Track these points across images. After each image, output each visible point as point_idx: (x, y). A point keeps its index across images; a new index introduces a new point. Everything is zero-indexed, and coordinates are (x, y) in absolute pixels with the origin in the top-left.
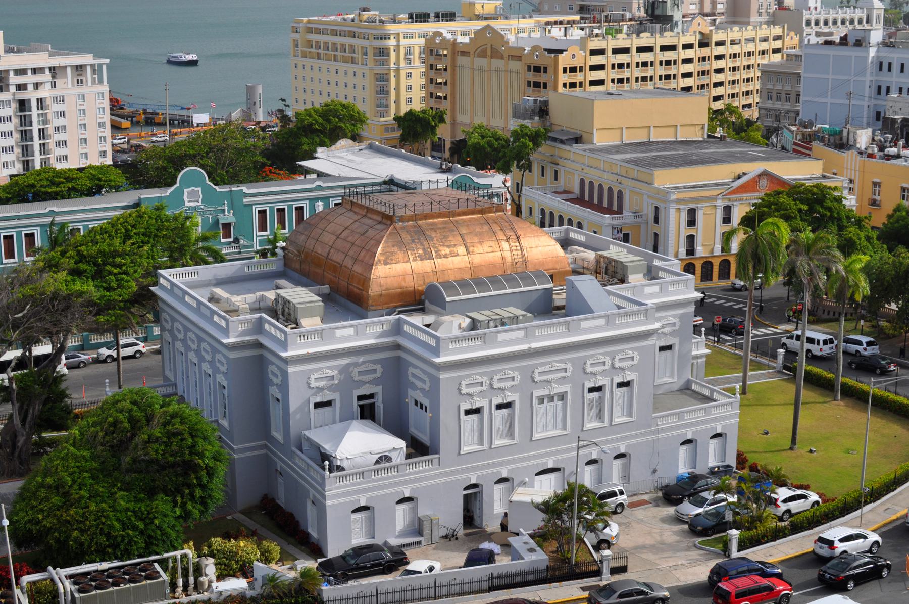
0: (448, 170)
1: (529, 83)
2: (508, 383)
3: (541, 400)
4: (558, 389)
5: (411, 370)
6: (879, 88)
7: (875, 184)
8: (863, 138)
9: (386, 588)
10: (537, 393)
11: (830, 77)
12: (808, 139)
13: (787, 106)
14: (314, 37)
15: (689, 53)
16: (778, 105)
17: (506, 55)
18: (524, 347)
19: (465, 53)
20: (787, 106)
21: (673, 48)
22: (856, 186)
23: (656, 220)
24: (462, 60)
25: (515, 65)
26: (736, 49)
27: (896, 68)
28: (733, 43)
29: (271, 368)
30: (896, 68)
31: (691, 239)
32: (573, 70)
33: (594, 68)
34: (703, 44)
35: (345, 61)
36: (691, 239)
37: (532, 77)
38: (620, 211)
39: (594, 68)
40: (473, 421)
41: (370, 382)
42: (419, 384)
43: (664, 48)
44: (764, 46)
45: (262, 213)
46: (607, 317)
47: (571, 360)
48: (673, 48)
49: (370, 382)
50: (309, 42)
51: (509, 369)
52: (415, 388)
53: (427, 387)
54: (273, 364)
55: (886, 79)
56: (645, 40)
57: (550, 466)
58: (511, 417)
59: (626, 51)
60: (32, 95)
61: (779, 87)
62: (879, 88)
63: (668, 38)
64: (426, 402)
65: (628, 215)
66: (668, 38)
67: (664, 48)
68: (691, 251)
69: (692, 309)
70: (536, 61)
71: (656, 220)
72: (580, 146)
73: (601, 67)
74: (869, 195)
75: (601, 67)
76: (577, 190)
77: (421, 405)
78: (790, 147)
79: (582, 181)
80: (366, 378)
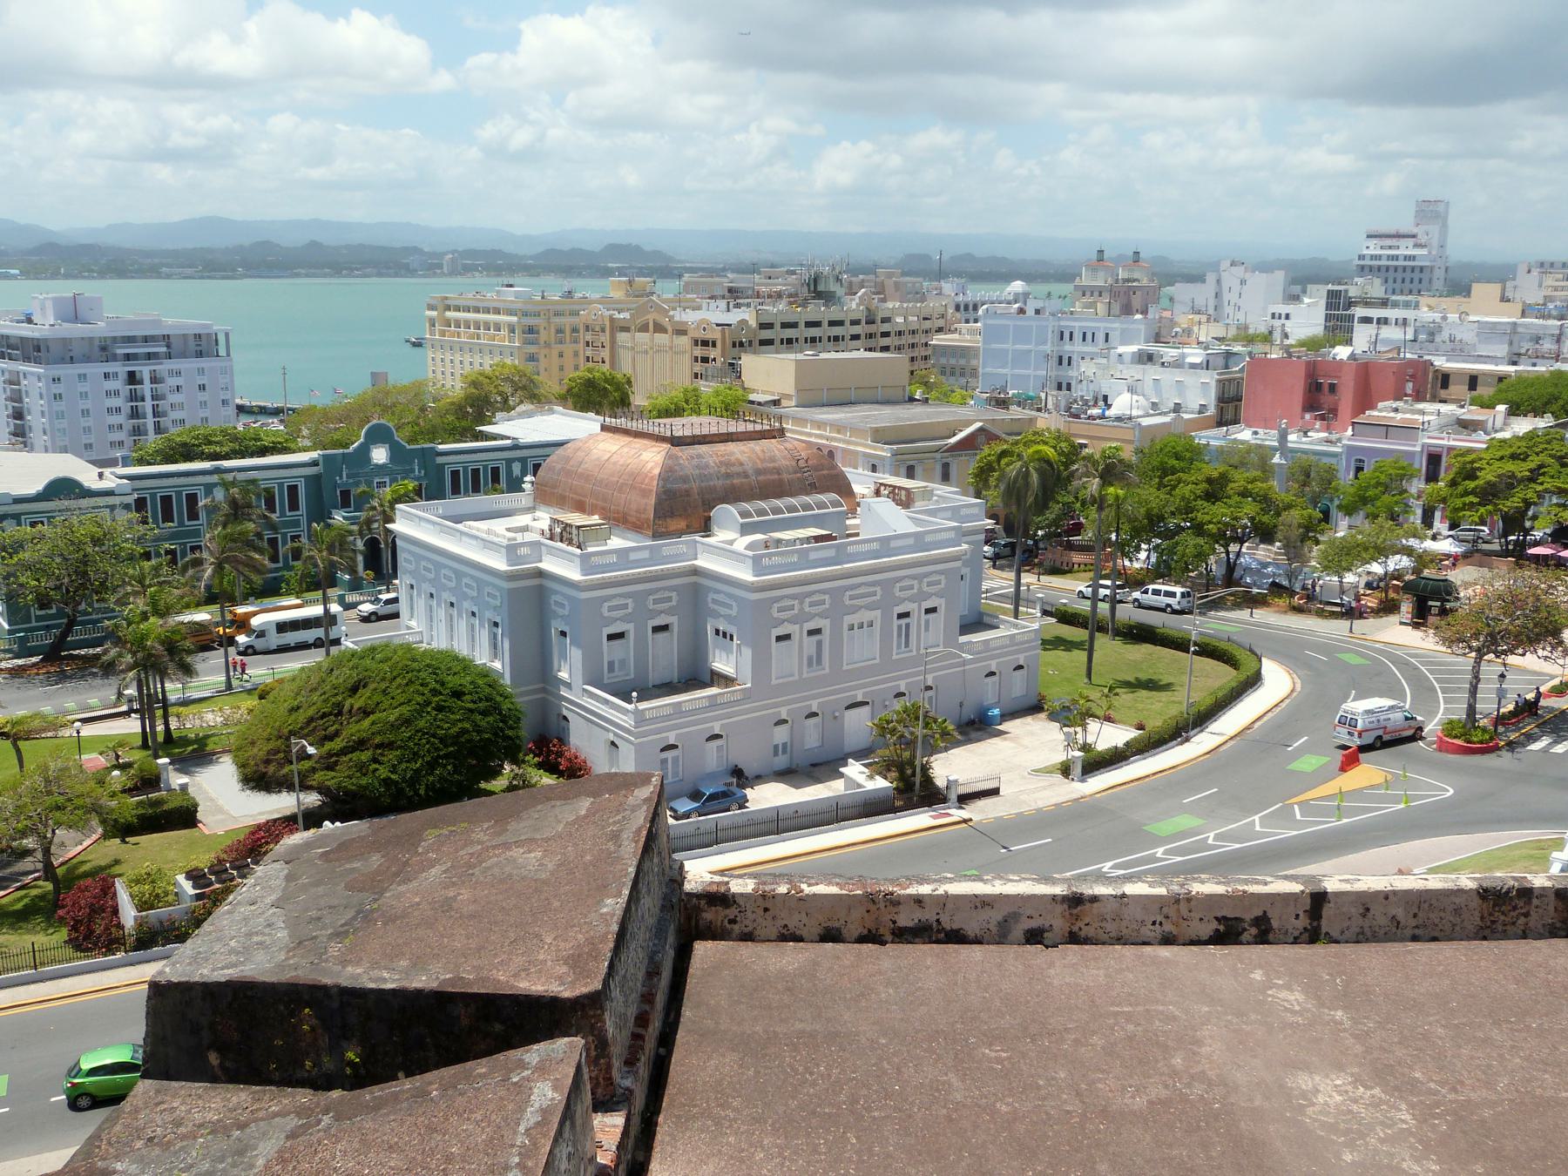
1: (696, 359)
4: (866, 616)
6: (1061, 358)
9: (726, 823)
15: (856, 330)
17: (670, 329)
19: (626, 329)
24: (622, 337)
25: (684, 341)
27: (1078, 336)
30: (1078, 336)
34: (870, 322)
37: (699, 352)
42: (723, 610)
45: (455, 474)
52: (717, 615)
53: (734, 613)
54: (557, 592)
58: (819, 644)
60: (145, 371)
62: (1061, 358)
64: (731, 629)
66: (834, 313)
69: (983, 537)
70: (701, 335)
77: (725, 635)
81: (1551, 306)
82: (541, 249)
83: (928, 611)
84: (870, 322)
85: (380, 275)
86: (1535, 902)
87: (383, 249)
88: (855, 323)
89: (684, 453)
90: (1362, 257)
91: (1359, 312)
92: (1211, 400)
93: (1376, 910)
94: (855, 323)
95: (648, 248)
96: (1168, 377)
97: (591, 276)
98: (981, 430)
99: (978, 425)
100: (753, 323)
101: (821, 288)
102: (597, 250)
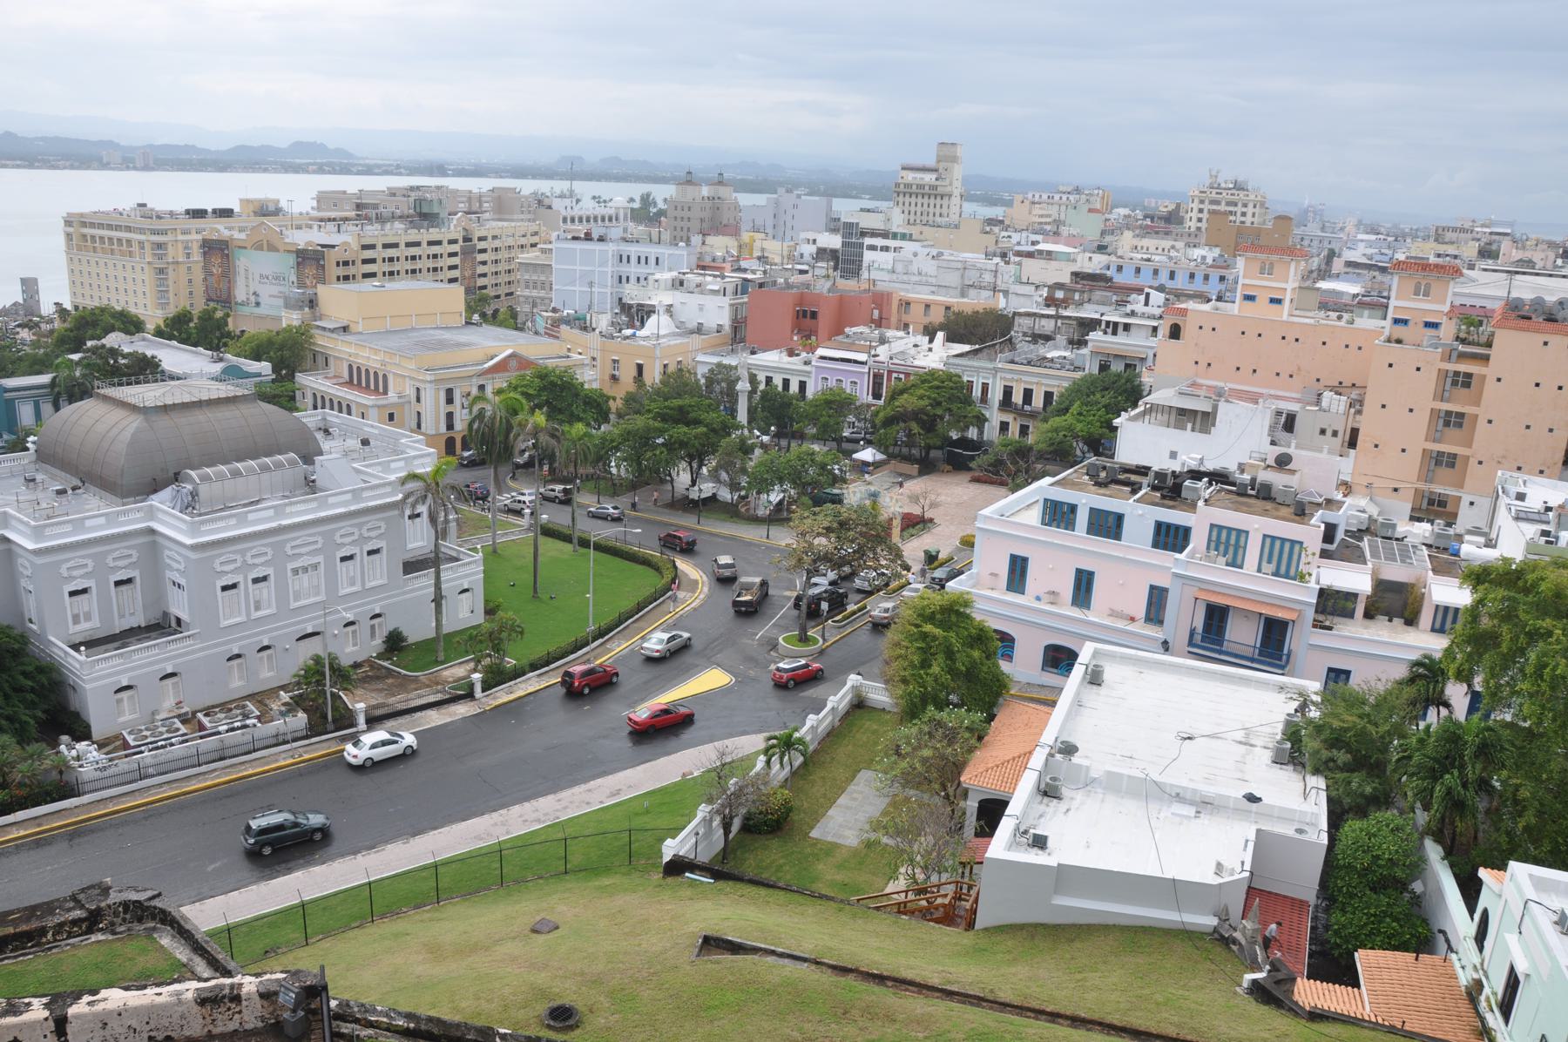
0: (221, 360)
2: (259, 559)
3: (295, 571)
5: (167, 552)
7: (614, 361)
8: (603, 322)
10: (290, 566)
11: (578, 268)
12: (556, 323)
13: (542, 294)
14: (88, 231)
16: (535, 293)
18: (274, 525)
20: (542, 294)
21: (439, 243)
22: (598, 363)
23: (418, 400)
26: (497, 243)
27: (634, 260)
28: (495, 237)
29: (20, 561)
30: (634, 260)
31: (450, 416)
32: (346, 263)
33: (365, 262)
35: (122, 254)
36: (450, 416)
38: (385, 392)
39: (365, 262)
40: (122, 616)
41: (82, 577)
42: (175, 565)
43: (430, 243)
44: (523, 241)
46: (353, 491)
47: (319, 533)
48: (439, 243)
49: (82, 577)
50: (84, 236)
51: (257, 546)
53: (182, 567)
55: (625, 269)
56: (413, 235)
57: (310, 630)
59: (418, 244)
61: (527, 277)
63: (434, 234)
64: (183, 582)
65: (392, 395)
66: (434, 234)
67: (430, 243)
68: (450, 427)
71: (418, 400)
72: (349, 338)
73: (373, 261)
74: (609, 371)
75: (373, 261)
76: (346, 375)
78: (542, 331)
79: (350, 367)
80: (121, 563)
81: (717, 388)
82: (231, 145)
83: (370, 553)
84: (467, 239)
85: (72, 167)
86: (244, 1003)
87: (78, 141)
88: (451, 242)
89: (163, 422)
90: (897, 185)
91: (868, 241)
92: (725, 319)
93: (114, 1024)
94: (451, 242)
95: (331, 146)
96: (694, 300)
97: (276, 171)
98: (510, 356)
99: (509, 352)
100: (355, 246)
101: (425, 210)
102: (284, 145)
